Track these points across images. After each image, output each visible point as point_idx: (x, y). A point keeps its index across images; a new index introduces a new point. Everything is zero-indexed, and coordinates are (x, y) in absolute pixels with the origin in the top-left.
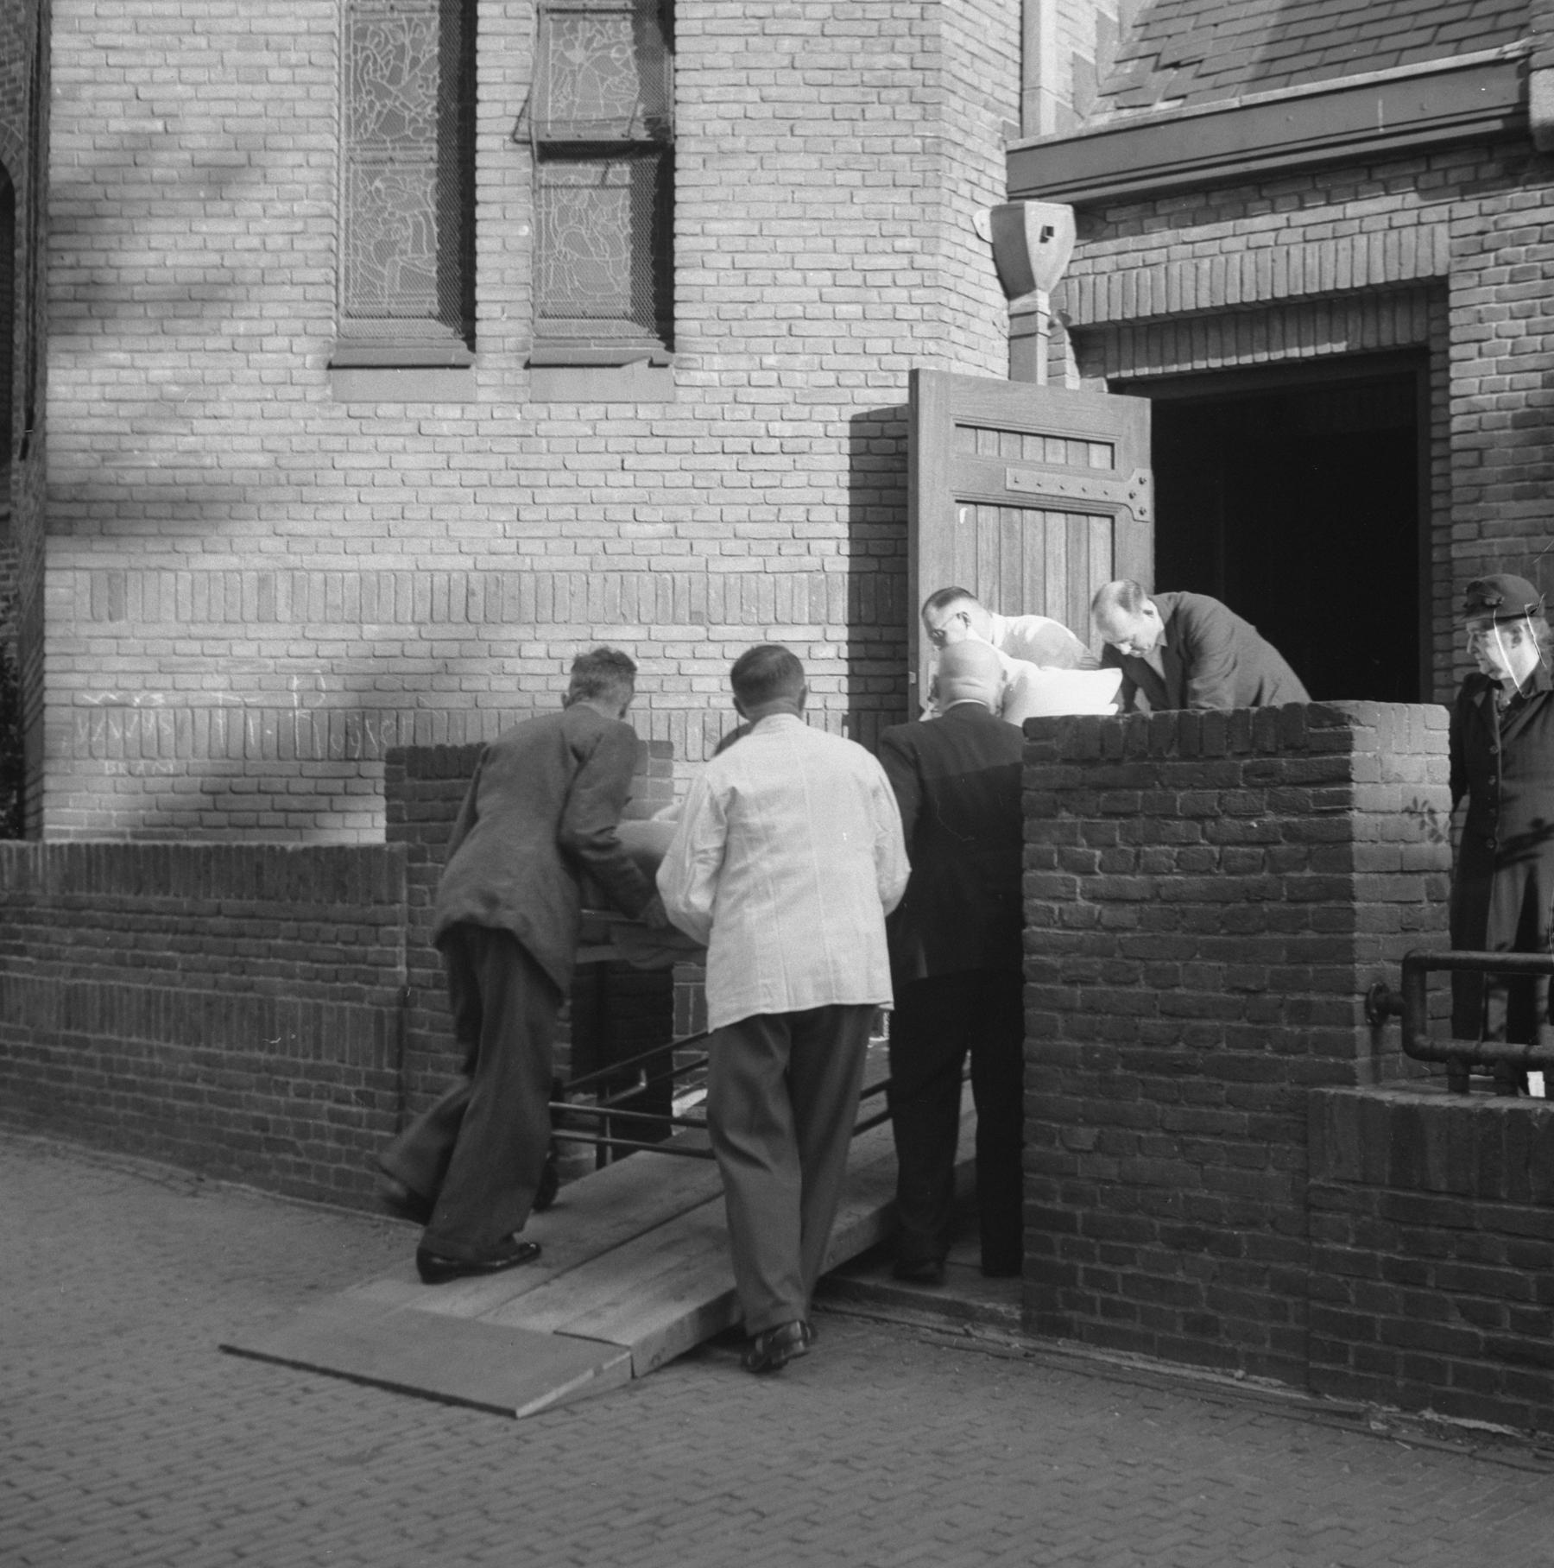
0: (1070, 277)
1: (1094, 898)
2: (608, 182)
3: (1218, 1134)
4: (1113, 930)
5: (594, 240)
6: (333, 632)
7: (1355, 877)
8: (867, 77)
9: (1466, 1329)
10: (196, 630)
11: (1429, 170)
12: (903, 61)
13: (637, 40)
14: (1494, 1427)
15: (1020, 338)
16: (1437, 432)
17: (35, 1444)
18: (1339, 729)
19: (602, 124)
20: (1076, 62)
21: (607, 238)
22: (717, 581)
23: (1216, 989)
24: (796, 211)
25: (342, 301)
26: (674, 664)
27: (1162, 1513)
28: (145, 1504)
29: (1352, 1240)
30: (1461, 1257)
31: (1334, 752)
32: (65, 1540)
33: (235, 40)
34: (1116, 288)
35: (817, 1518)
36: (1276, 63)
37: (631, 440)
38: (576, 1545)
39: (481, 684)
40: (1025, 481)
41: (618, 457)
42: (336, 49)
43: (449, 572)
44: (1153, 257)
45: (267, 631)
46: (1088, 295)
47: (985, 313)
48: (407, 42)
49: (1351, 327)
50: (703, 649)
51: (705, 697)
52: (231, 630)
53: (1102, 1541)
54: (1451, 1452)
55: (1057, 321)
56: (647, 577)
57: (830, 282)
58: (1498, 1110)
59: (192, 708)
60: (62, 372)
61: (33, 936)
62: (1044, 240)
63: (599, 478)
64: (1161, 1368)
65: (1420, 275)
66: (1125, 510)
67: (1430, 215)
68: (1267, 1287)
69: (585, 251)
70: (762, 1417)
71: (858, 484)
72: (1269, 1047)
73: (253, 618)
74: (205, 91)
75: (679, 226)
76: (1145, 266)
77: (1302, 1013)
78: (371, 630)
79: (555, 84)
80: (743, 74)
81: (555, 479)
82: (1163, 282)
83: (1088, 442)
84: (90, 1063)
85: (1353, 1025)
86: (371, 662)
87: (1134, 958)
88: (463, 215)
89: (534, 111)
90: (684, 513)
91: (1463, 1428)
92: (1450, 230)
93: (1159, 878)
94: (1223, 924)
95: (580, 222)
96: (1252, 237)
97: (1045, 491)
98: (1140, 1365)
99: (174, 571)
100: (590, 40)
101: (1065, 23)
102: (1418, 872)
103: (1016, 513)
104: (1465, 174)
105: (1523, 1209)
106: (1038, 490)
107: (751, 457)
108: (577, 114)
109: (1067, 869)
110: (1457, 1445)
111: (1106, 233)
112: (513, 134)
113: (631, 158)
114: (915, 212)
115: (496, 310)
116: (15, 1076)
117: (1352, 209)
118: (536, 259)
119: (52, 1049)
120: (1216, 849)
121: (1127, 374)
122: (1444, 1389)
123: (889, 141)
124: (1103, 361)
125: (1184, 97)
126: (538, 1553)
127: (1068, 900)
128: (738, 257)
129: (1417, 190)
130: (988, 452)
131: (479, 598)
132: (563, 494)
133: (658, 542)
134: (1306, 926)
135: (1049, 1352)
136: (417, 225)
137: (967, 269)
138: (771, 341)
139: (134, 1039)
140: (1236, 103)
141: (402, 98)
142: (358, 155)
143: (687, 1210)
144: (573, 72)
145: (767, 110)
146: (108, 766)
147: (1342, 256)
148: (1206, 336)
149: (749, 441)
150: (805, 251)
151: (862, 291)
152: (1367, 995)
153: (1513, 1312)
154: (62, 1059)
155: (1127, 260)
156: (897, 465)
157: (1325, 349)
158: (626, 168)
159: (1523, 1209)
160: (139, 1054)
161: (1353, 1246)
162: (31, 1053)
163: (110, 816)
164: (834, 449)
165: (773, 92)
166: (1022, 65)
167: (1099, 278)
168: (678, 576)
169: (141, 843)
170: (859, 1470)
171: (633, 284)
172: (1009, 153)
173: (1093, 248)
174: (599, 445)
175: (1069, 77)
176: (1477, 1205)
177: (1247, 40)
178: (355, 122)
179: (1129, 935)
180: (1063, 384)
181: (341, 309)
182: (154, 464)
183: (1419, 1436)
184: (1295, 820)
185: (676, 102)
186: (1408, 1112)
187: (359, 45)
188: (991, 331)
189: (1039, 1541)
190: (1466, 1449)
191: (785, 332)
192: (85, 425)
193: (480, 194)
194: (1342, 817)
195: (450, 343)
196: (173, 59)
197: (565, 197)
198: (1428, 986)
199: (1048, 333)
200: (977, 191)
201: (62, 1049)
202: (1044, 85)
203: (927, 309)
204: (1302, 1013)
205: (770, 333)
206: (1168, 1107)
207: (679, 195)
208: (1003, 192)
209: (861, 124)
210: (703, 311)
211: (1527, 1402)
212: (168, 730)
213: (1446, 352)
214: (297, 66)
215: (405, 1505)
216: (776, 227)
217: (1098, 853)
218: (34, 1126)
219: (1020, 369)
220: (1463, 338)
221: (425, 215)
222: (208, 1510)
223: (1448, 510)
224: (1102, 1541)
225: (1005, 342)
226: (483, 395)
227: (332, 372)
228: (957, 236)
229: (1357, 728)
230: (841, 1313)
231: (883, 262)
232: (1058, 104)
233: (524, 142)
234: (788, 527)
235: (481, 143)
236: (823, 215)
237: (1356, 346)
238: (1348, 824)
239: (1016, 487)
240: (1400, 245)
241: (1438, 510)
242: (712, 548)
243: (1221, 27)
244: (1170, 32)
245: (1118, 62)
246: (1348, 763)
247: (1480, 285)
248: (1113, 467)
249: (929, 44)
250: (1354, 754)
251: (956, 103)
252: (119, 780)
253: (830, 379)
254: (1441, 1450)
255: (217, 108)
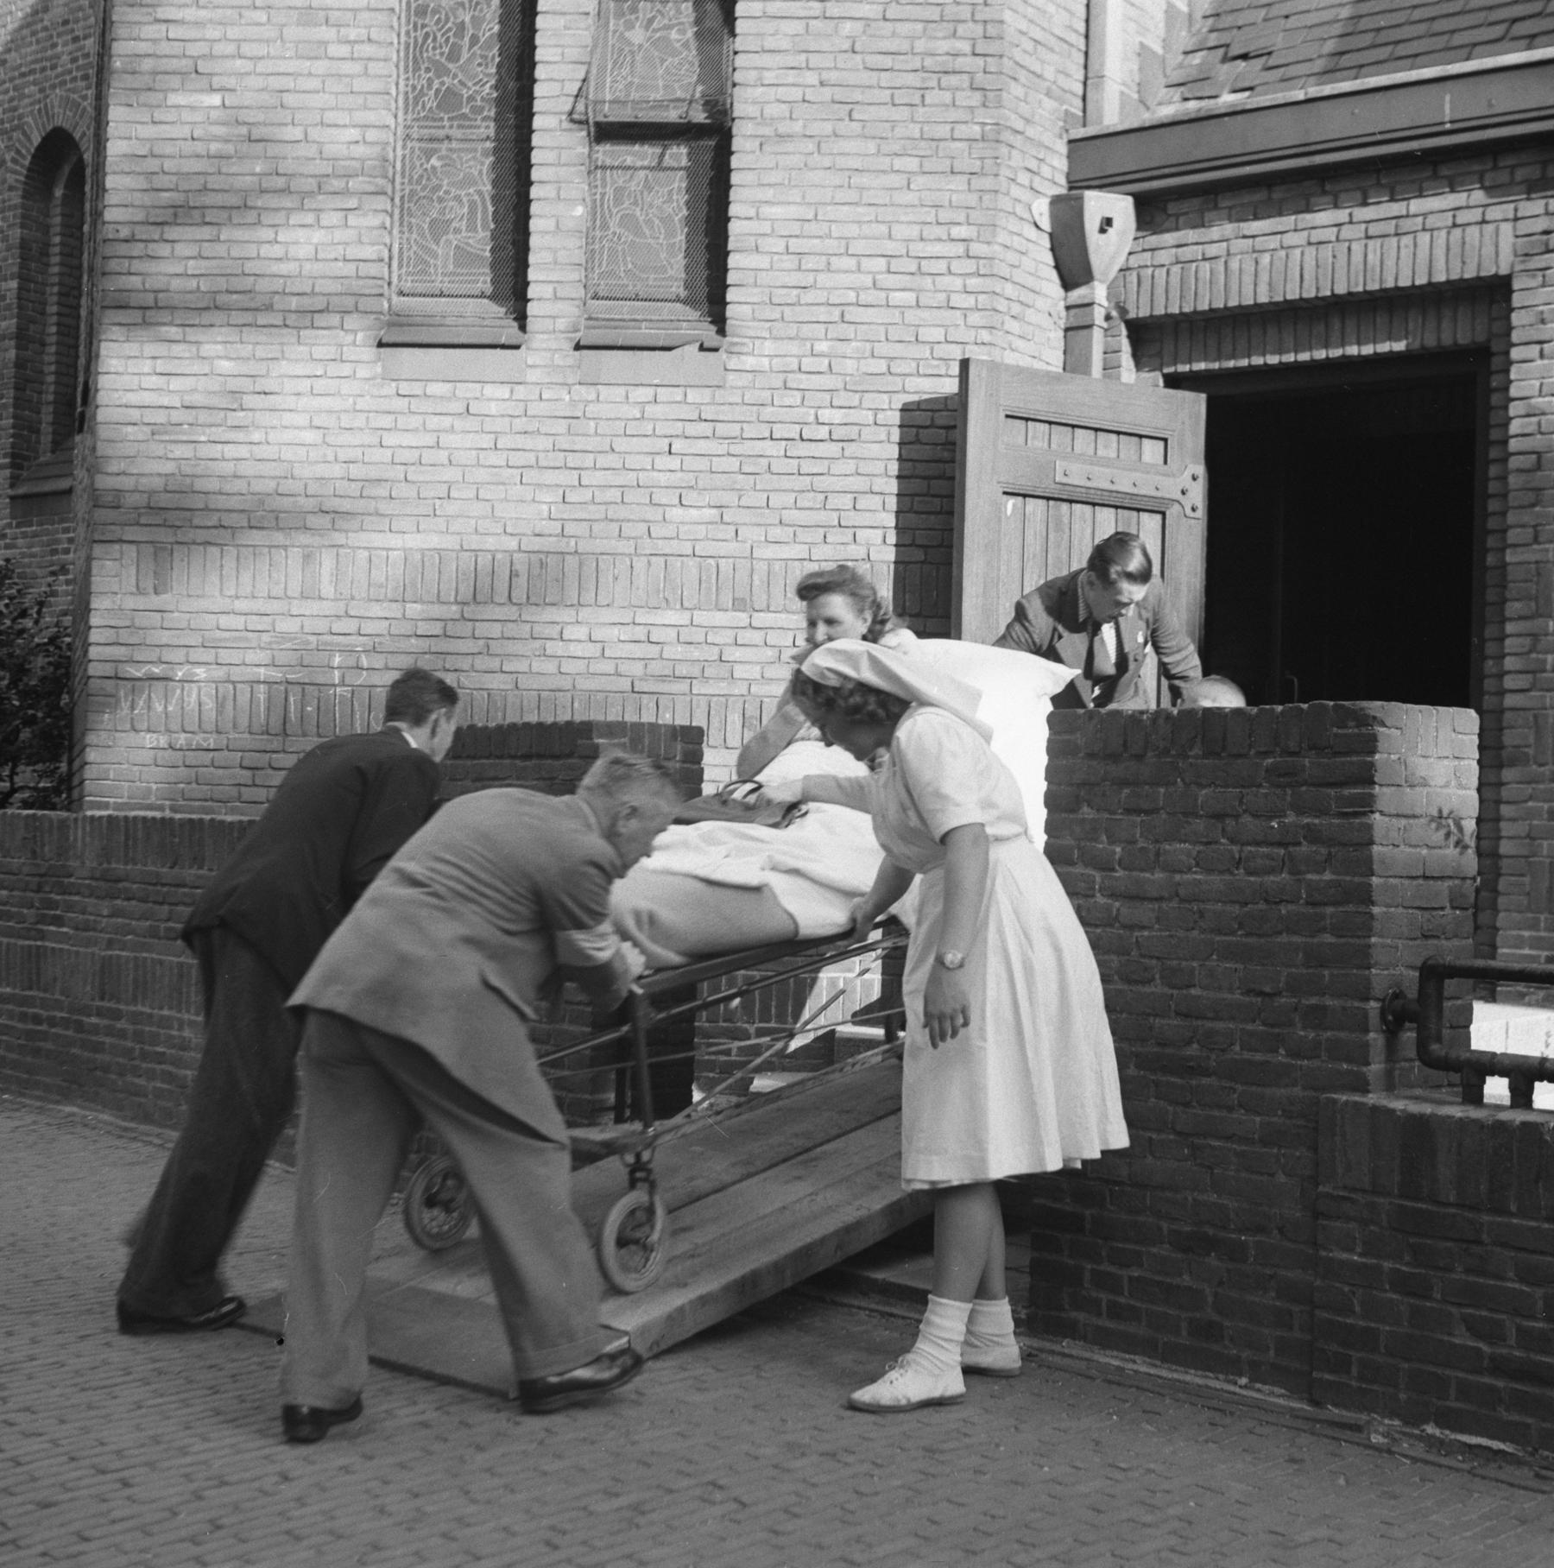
0: (1128, 269)
1: (1113, 896)
2: (665, 164)
3: (1229, 1138)
4: (1131, 927)
5: (649, 222)
6: (376, 610)
7: (1375, 880)
8: (928, 62)
9: (1471, 1343)
10: (241, 605)
11: (1495, 168)
12: (965, 47)
13: (698, 22)
14: (1496, 1445)
15: (1076, 329)
16: (1495, 435)
17: (27, 1409)
18: (1364, 730)
19: (659, 105)
20: (1143, 52)
21: (661, 219)
22: (761, 567)
23: (1231, 990)
24: (852, 196)
25: (395, 280)
26: (716, 650)
27: (1149, 1518)
28: (126, 1474)
29: (1359, 1250)
30: (1468, 1271)
31: (1357, 753)
32: (46, 1505)
33: (294, 14)
34: (1175, 280)
35: (796, 1510)
36: (1345, 57)
37: (680, 424)
38: (553, 1528)
39: (522, 666)
40: (1076, 474)
41: (667, 441)
42: (396, 25)
43: (493, 553)
44: (1212, 250)
45: (313, 607)
46: (1146, 285)
47: (1040, 303)
48: (467, 19)
49: (1411, 326)
50: (747, 636)
51: (746, 684)
52: (275, 606)
53: (1084, 1544)
54: (1450, 1468)
55: (1114, 313)
56: (691, 562)
57: (884, 269)
58: (1512, 1122)
59: (233, 683)
60: (116, 345)
61: (70, 907)
62: (1102, 231)
63: (646, 462)
64: (1164, 1373)
65: (1483, 274)
66: (1176, 507)
67: (1494, 213)
68: (1273, 1294)
69: (638, 231)
70: (755, 1407)
71: (905, 473)
72: (1282, 1051)
73: (297, 595)
74: (261, 67)
75: (733, 210)
76: (1204, 259)
77: (1316, 1018)
78: (414, 609)
79: (615, 63)
80: (803, 57)
81: (603, 461)
82: (1222, 277)
83: (1141, 436)
84: (122, 1034)
85: (1367, 1031)
86: (413, 640)
87: (1151, 957)
88: (518, 194)
89: (592, 90)
90: (729, 498)
91: (1465, 1444)
92: (1515, 228)
93: (1178, 877)
94: (1241, 926)
95: (635, 203)
96: (1313, 232)
97: (1143, 492)
98: (1143, 1369)
99: (285, 547)
100: (651, 21)
101: (1133, 12)
102: (1442, 878)
103: (1065, 507)
104: (1533, 172)
105: (1533, 1224)
106: (1089, 484)
107: (800, 444)
108: (634, 95)
109: (1086, 865)
110: (1457, 1461)
111: (1167, 225)
112: (571, 113)
113: (688, 140)
114: (972, 199)
115: (547, 291)
116: (49, 1046)
117: (1416, 205)
118: (589, 239)
119: (85, 1019)
120: (1235, 848)
121: (1183, 368)
122: (1448, 1403)
123: (948, 127)
124: (1160, 354)
125: (1251, 89)
126: (514, 1534)
127: (1087, 896)
128: (792, 241)
129: (1483, 188)
130: (1038, 444)
131: (522, 581)
132: (609, 478)
133: (703, 527)
134: (1323, 930)
135: (1052, 1352)
136: (472, 205)
137: (1024, 258)
138: (823, 326)
139: (166, 1012)
140: (1300, 95)
141: (460, 76)
142: (415, 132)
143: (698, 1199)
144: (632, 53)
145: (827, 93)
146: (149, 740)
147: (1403, 252)
148: (1265, 333)
149: (798, 427)
150: (859, 237)
151: (917, 278)
152: (1383, 1000)
153: (1519, 1329)
154: (95, 1030)
155: (1186, 253)
156: (946, 455)
157: (1384, 347)
158: (684, 150)
159: (1533, 1224)
160: (170, 1028)
161: (1360, 1255)
162: (66, 1023)
163: (149, 790)
164: (883, 437)
165: (833, 76)
166: (1086, 53)
167: (1157, 271)
168: (722, 562)
169: (178, 816)
170: (846, 1464)
171: (687, 267)
172: (1070, 142)
173: (1153, 240)
174: (648, 428)
175: (1136, 67)
176: (1486, 1218)
177: (1317, 32)
178: (414, 99)
179: (1146, 933)
180: (1118, 378)
181: (393, 287)
182: (203, 438)
183: (1419, 1450)
184: (1317, 821)
185: (734, 85)
186: (1420, 1124)
187: (420, 22)
188: (1047, 322)
189: (1019, 1541)
190: (1466, 1466)
191: (836, 318)
192: (132, 398)
193: (535, 174)
194: (1364, 820)
195: (499, 322)
196: (233, 33)
197: (620, 178)
198: (1446, 994)
199: (1105, 325)
200: (1037, 179)
201: (94, 1020)
202: (1106, 73)
203: (981, 298)
204: (1316, 1018)
205: (821, 319)
206: (1179, 1109)
207: (735, 178)
208: (1063, 181)
209: (921, 110)
210: (754, 295)
211: (1529, 1420)
212: (210, 705)
213: (1507, 353)
214: (356, 42)
215: (386, 1483)
216: (831, 212)
217: (1118, 850)
218: (66, 1096)
219: (1075, 361)
220: (1524, 340)
221: (480, 193)
222: (191, 1481)
223: (1504, 514)
224: (1084, 1544)
225: (1061, 334)
226: (533, 376)
227: (382, 350)
228: (1013, 225)
229: (1382, 729)
230: (852, 1306)
231: (938, 249)
232: (1122, 93)
233: (580, 122)
234: (835, 515)
235: (537, 122)
236: (881, 202)
237: (1417, 345)
238: (1370, 827)
239: (1065, 480)
240: (1464, 243)
241: (1494, 514)
242: (756, 534)
243: (1223, 17)
244: (1240, 23)
245: (1186, 53)
246: (1372, 765)
247: (1544, 285)
248: (1166, 462)
249: (992, 30)
250: (1377, 756)
251: (1017, 90)
252: (160, 753)
253: (881, 366)
254: (1440, 1466)
255: (275, 82)
